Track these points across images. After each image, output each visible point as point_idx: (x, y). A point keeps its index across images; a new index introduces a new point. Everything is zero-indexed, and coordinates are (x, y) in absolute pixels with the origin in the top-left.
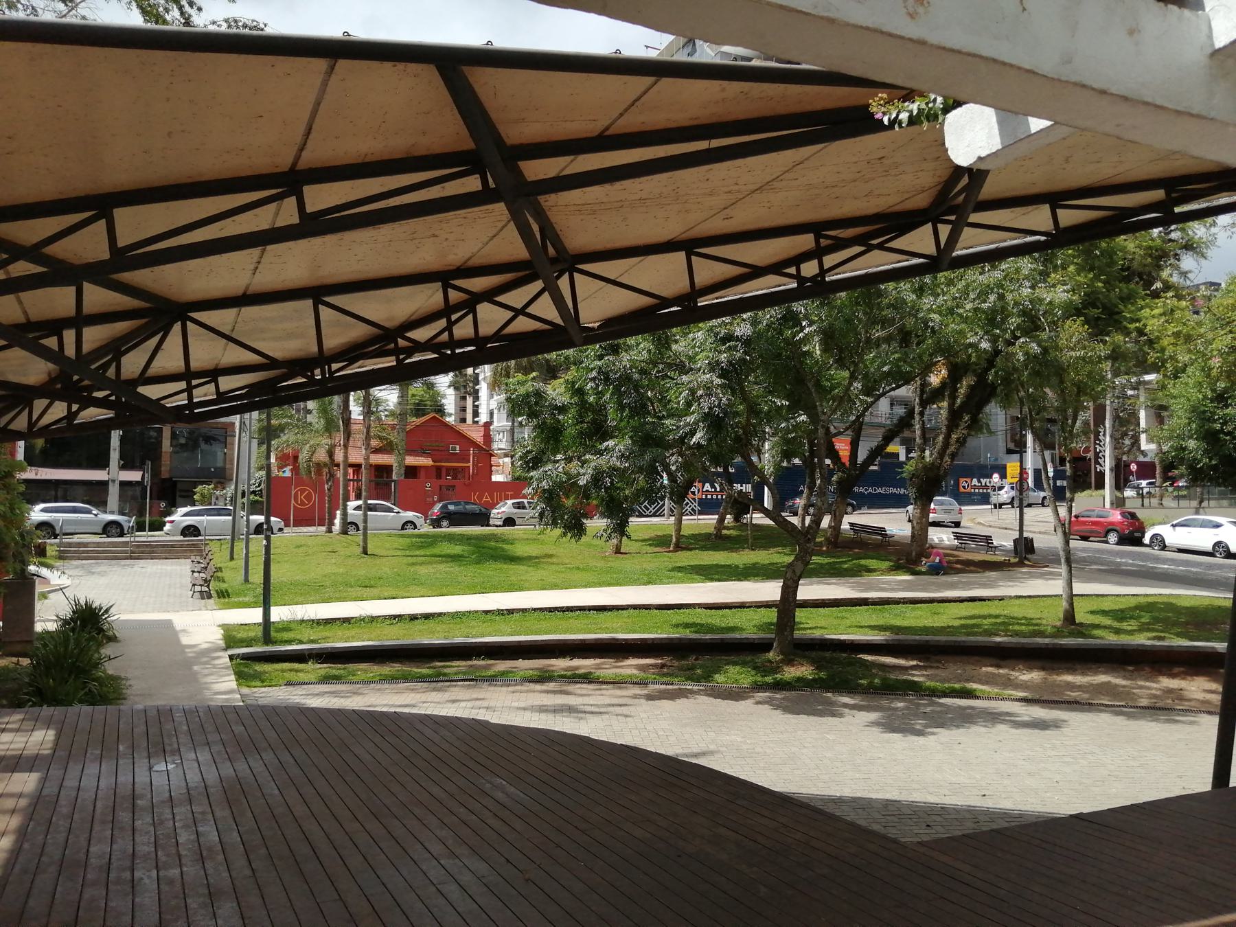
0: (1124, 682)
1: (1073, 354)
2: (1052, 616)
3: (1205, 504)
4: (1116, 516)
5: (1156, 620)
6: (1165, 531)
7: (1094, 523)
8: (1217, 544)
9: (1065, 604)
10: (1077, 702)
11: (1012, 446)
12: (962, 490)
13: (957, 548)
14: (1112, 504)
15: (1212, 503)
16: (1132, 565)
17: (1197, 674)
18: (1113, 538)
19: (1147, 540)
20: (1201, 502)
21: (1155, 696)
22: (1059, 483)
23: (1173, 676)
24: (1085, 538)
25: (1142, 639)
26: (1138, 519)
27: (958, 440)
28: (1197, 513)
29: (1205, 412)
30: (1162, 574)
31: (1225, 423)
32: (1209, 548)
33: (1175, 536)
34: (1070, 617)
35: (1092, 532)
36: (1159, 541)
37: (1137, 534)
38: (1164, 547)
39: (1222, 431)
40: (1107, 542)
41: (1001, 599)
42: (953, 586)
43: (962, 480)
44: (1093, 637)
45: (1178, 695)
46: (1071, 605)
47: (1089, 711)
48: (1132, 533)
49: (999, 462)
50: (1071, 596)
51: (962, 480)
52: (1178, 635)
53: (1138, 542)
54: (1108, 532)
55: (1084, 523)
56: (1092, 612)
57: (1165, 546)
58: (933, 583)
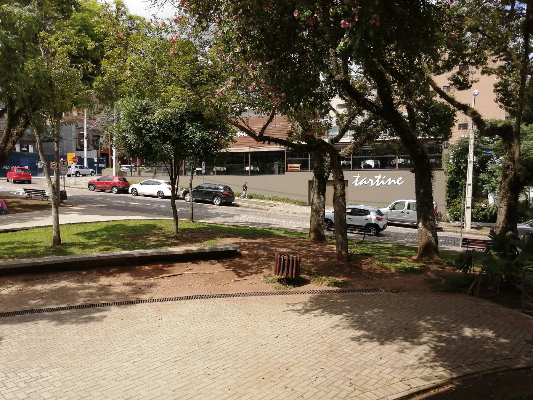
0: (74, 285)
1: (57, 71)
2: (47, 240)
3: (157, 174)
4: (116, 180)
5: (111, 236)
6: (137, 186)
7: (107, 183)
8: (159, 192)
9: (54, 233)
10: (31, 311)
11: (79, 147)
12: (51, 167)
13: (26, 198)
14: (116, 174)
15: (160, 174)
16: (119, 203)
17: (123, 271)
18: (115, 190)
19: (130, 191)
20: (155, 173)
21: (91, 294)
22: (100, 165)
23: (109, 275)
24: (103, 191)
25: (96, 253)
26: (127, 181)
27: (17, 134)
28: (153, 178)
29: (135, 117)
30: (132, 207)
31: (145, 124)
32: (155, 193)
33: (142, 189)
34: (57, 240)
35: (105, 187)
36: (135, 192)
37: (126, 188)
38: (137, 194)
39: (144, 128)
40: (112, 192)
41: (27, 229)
42: (12, 221)
43: (51, 163)
44: (67, 254)
45: (105, 290)
46: (58, 232)
47: (33, 320)
48: (124, 187)
49: (65, 154)
50: (58, 226)
51: (51, 163)
52: (118, 246)
53: (126, 192)
54: (113, 187)
55: (102, 183)
56: (78, 234)
57: (138, 194)
58: (8, 220)
